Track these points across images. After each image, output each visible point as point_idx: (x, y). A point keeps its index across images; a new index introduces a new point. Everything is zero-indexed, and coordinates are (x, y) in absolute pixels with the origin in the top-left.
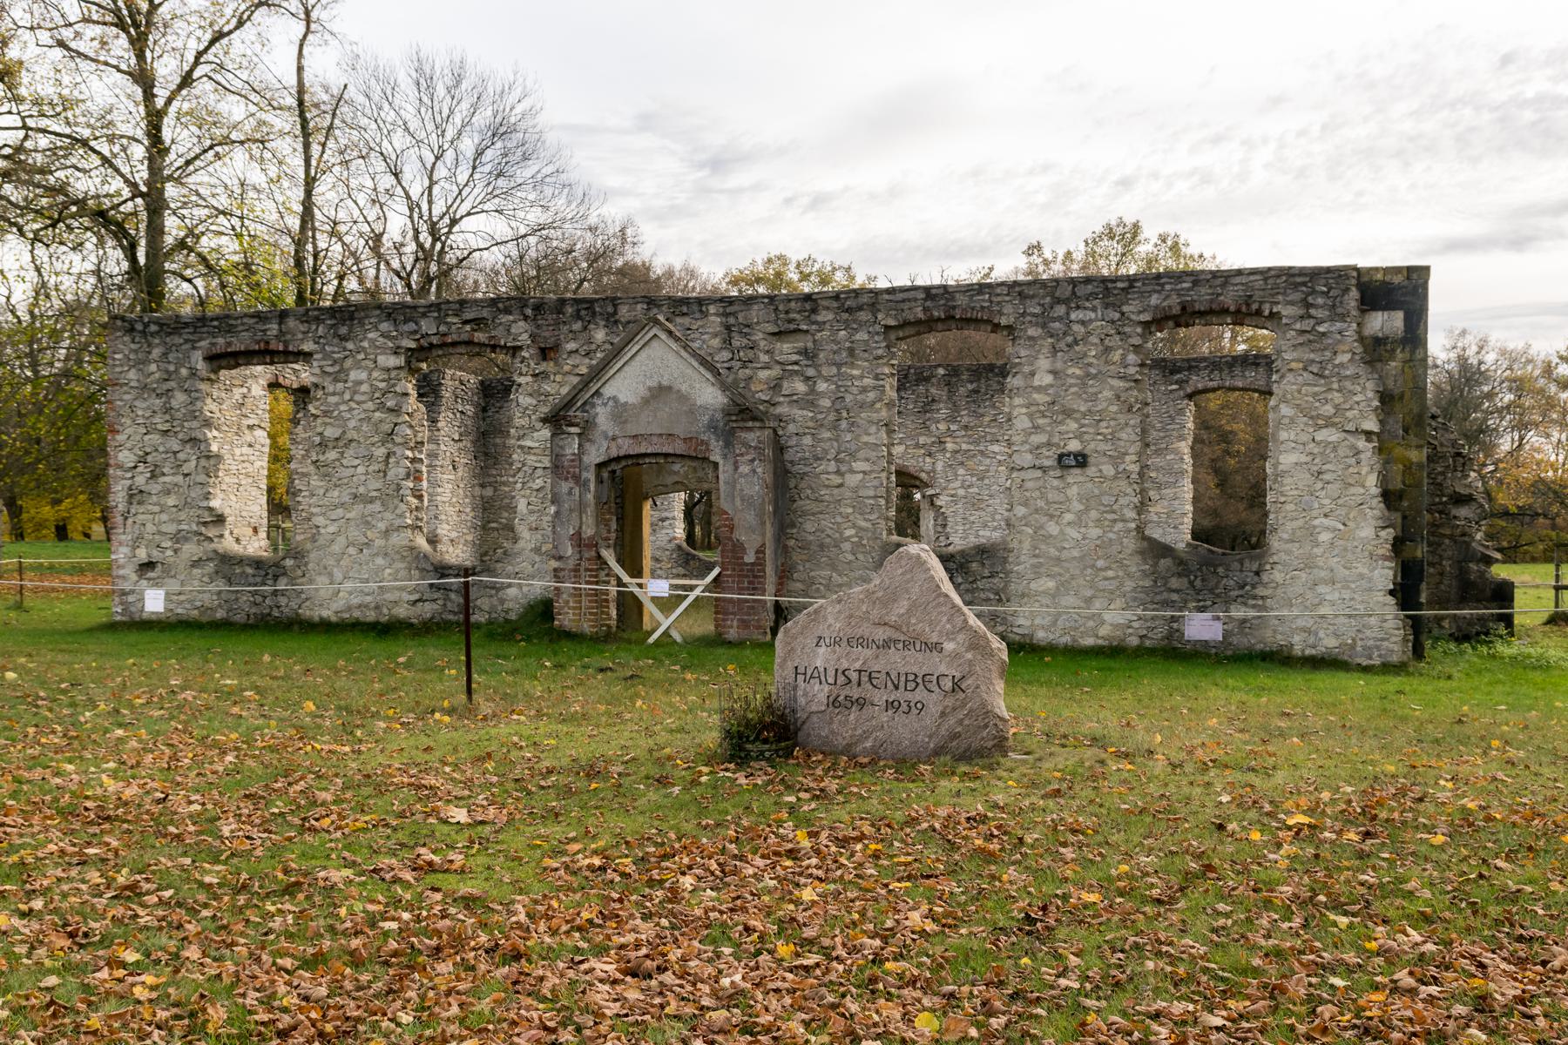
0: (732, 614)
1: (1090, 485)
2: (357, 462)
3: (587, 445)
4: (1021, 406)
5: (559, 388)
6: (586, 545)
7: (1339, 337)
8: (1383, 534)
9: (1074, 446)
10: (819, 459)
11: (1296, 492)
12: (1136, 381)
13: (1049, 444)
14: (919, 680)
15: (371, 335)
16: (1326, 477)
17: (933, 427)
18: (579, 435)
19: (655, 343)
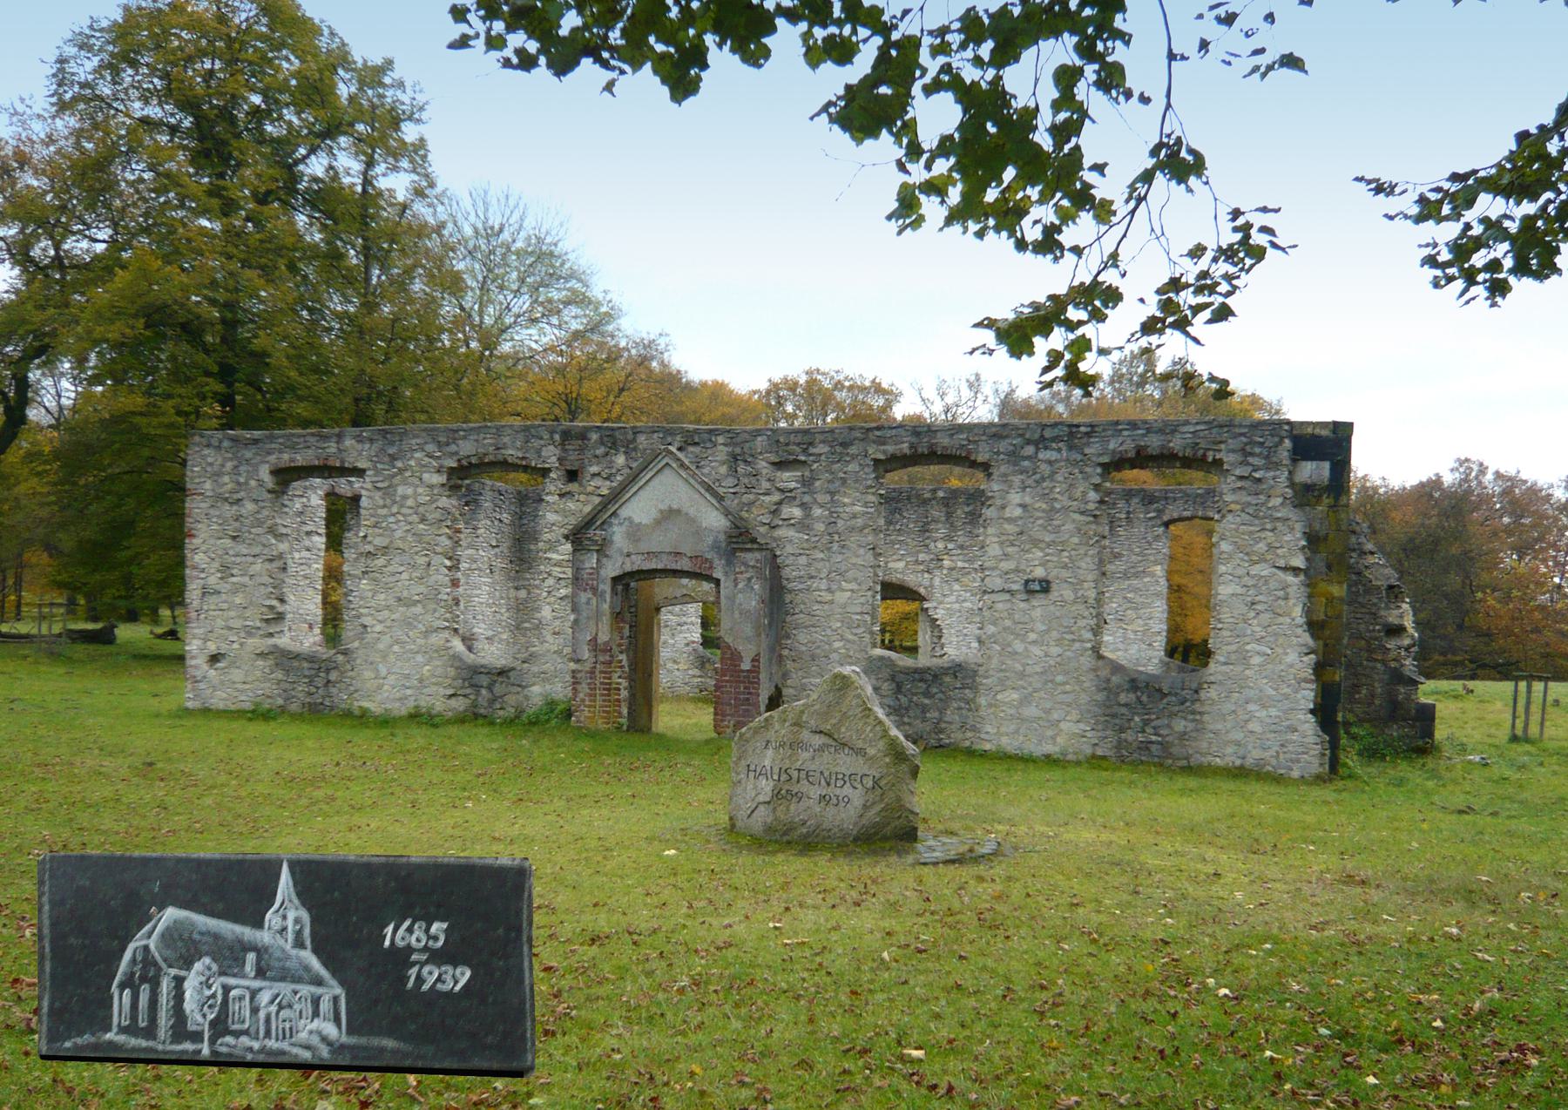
1: (1052, 608)
2: (402, 569)
4: (994, 535)
5: (580, 507)
7: (1272, 482)
8: (1305, 659)
9: (1039, 572)
10: (812, 577)
11: (1231, 620)
12: (1095, 516)
13: (1017, 570)
14: (846, 778)
15: (417, 455)
16: (1259, 607)
17: (932, 546)
18: (598, 551)
19: (667, 471)
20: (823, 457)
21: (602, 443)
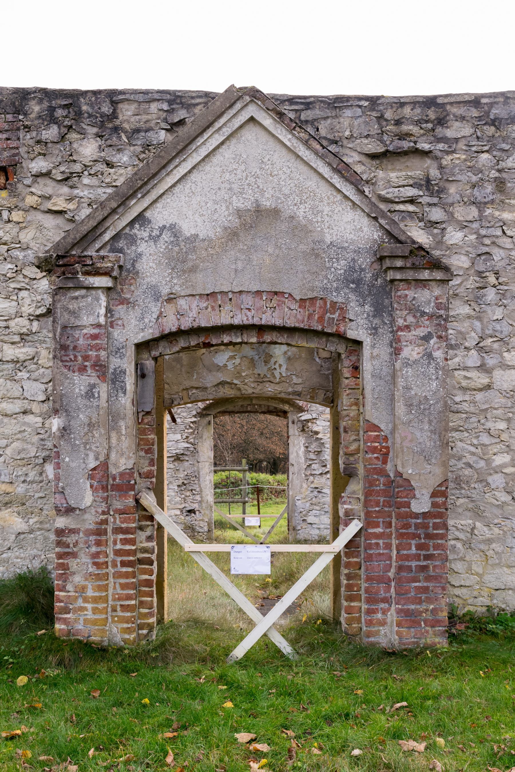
0: (385, 600)
3: (120, 310)
6: (117, 488)
20: (461, 145)
21: (53, 120)
